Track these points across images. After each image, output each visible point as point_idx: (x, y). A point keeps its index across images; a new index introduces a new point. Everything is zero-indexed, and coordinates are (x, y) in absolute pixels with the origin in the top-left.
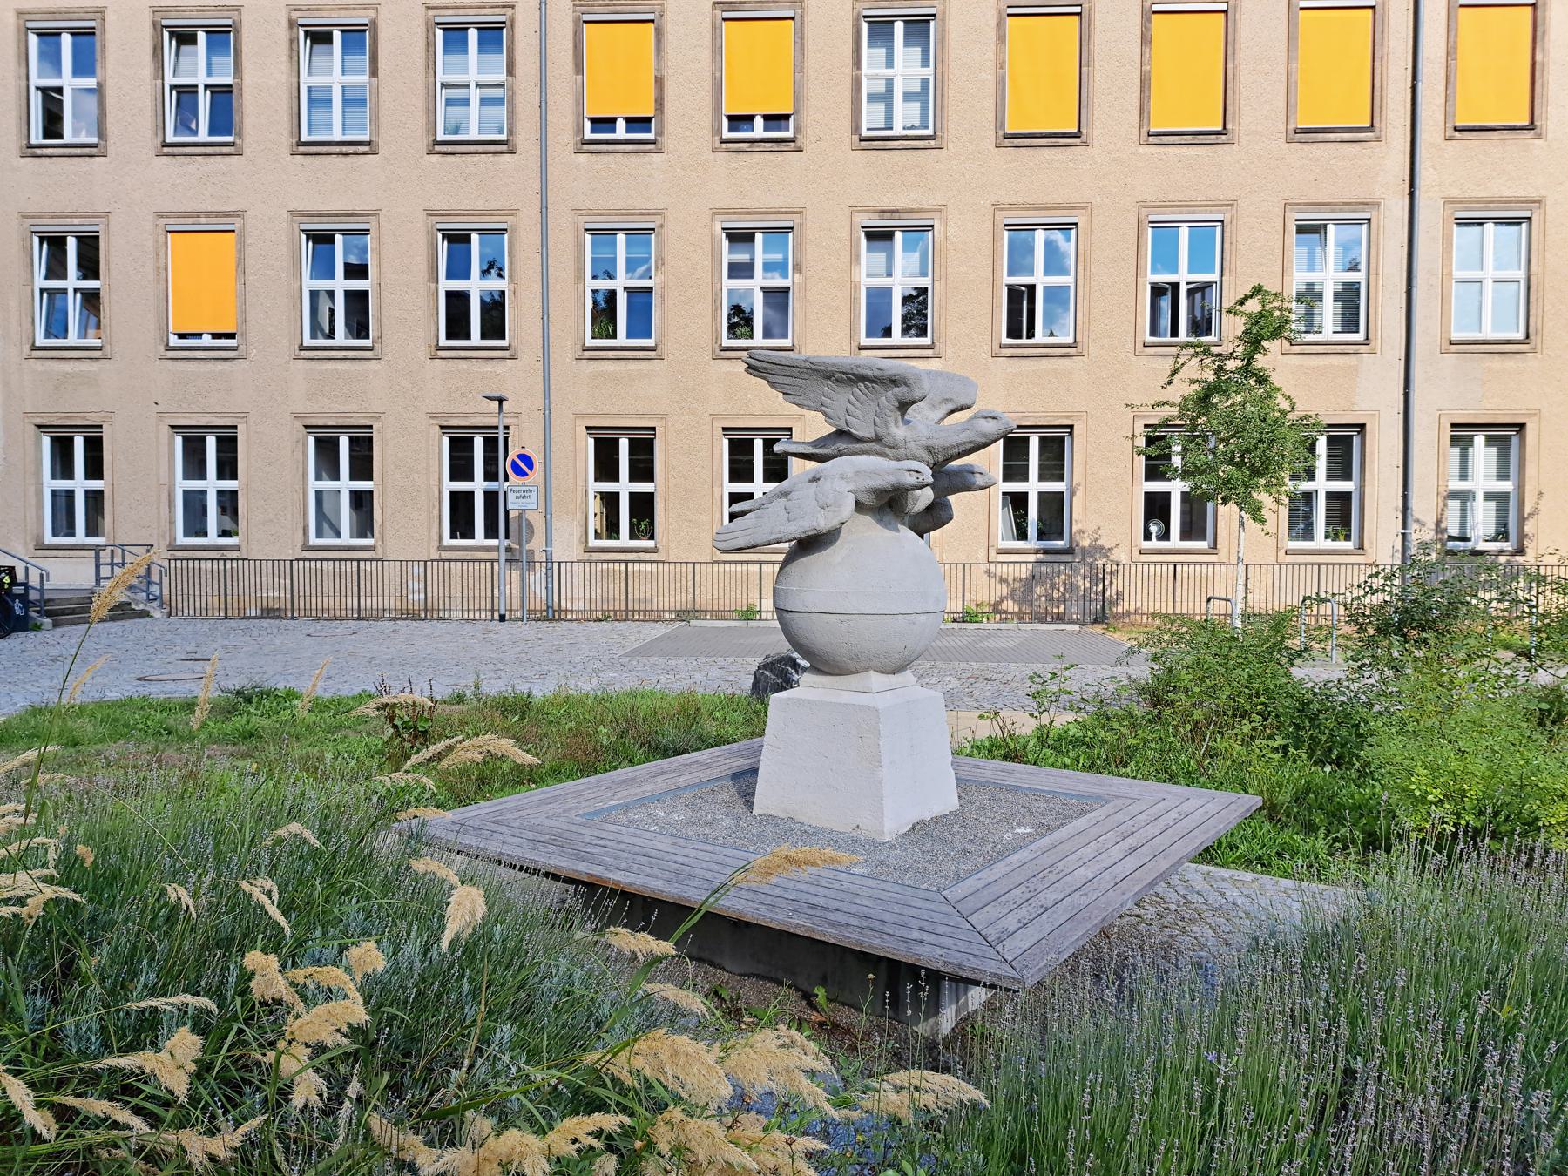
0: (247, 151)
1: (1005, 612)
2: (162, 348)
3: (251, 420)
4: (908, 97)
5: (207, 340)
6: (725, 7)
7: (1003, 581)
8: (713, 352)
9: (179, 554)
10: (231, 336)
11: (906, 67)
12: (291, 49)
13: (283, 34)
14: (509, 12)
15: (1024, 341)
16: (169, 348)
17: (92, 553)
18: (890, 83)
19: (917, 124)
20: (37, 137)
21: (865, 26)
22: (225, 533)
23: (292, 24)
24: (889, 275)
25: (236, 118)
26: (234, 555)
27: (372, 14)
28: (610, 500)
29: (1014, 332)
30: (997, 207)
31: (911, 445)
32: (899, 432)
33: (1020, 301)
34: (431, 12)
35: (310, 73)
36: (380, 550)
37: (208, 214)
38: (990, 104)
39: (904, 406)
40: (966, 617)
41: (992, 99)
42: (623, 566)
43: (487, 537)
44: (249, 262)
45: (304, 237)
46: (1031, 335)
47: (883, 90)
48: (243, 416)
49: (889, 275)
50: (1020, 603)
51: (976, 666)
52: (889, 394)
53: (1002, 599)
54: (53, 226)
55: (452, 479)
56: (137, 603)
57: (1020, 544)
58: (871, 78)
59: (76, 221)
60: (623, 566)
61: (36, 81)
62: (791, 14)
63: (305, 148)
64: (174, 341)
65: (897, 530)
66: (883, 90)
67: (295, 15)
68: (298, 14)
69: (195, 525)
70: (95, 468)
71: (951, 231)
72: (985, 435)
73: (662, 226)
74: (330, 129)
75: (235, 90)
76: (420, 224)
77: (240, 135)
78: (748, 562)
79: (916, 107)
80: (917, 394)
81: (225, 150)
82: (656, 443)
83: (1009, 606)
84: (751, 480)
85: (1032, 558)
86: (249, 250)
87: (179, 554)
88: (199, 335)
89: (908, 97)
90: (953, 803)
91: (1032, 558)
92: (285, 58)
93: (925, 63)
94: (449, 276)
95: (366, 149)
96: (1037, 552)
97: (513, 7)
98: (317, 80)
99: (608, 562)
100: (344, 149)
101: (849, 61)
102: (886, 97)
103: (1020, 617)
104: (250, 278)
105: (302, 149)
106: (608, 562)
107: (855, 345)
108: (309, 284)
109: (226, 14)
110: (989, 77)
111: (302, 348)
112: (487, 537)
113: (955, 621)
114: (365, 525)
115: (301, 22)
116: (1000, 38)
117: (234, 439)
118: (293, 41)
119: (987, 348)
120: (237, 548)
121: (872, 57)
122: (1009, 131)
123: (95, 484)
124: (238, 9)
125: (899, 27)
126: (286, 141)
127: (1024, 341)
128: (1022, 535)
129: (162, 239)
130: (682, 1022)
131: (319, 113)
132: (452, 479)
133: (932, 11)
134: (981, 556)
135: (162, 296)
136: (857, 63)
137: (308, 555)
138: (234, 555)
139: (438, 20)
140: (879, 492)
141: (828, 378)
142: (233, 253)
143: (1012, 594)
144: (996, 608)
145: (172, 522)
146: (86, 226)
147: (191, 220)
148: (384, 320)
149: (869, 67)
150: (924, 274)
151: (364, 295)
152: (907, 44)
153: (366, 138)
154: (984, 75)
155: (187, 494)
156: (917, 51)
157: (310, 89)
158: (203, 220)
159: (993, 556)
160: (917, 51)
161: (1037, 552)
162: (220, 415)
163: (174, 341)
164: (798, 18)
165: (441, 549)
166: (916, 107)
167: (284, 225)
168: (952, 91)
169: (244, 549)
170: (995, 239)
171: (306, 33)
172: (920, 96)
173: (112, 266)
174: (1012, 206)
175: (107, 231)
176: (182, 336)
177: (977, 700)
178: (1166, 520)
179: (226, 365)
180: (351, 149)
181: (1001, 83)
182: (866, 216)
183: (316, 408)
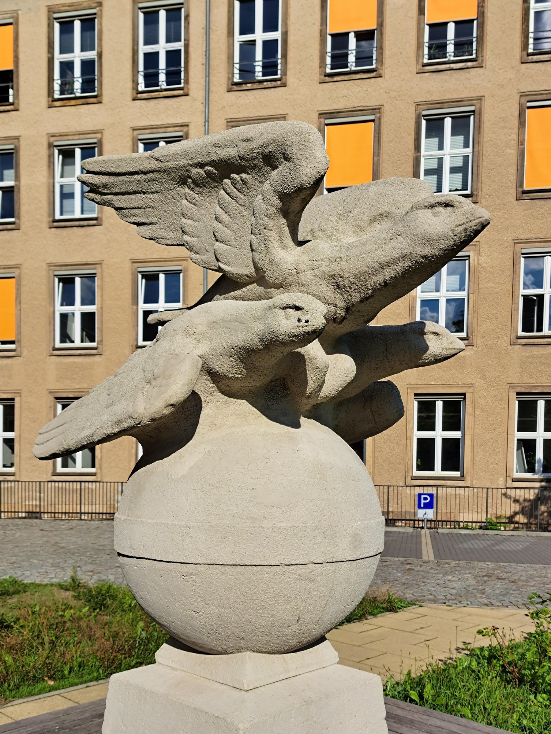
0: (23, 227)
1: (517, 523)
3: (23, 395)
4: (453, 170)
6: (327, 116)
7: (516, 501)
10: (12, 342)
11: (453, 149)
12: (49, 162)
13: (44, 152)
14: (185, 129)
15: (535, 334)
18: (440, 160)
19: (460, 188)
21: (424, 123)
23: (51, 146)
24: (437, 290)
25: (16, 207)
27: (99, 136)
29: (527, 327)
30: (517, 242)
31: (307, 277)
32: (286, 257)
33: (533, 306)
34: (136, 132)
35: (62, 176)
36: (99, 475)
38: (513, 170)
39: (294, 203)
40: (488, 526)
41: (515, 167)
44: (23, 296)
45: (56, 280)
46: (540, 329)
47: (435, 166)
48: (19, 393)
49: (437, 290)
50: (529, 518)
51: (491, 565)
52: (266, 186)
53: (516, 513)
57: (529, 475)
58: (427, 158)
62: (372, 117)
63: (57, 224)
65: (297, 425)
66: (435, 166)
67: (52, 139)
68: (53, 139)
71: (482, 259)
72: (428, 240)
74: (73, 212)
75: (15, 189)
76: (127, 267)
77: (19, 218)
78: (447, 487)
79: (459, 176)
80: (306, 174)
81: (9, 227)
83: (521, 518)
85: (537, 485)
86: (23, 289)
89: (453, 170)
91: (537, 485)
92: (45, 167)
93: (466, 145)
94: (146, 302)
95: (94, 222)
96: (541, 481)
97: (187, 126)
98: (65, 181)
100: (81, 223)
101: (412, 146)
102: (437, 172)
103: (528, 526)
104: (23, 306)
105: (56, 224)
108: (60, 309)
109: (11, 141)
110: (512, 152)
113: (481, 528)
115: (56, 143)
116: (522, 123)
118: (51, 157)
119: (507, 339)
120: (13, 474)
121: (428, 146)
122: (526, 188)
124: (17, 138)
125: (448, 122)
126: (45, 219)
127: (535, 334)
128: (531, 469)
131: (66, 202)
133: (472, 108)
134: (501, 482)
136: (417, 147)
139: (141, 137)
140: (247, 355)
141: (183, 182)
142: (14, 291)
143: (523, 511)
144: (511, 519)
148: (104, 330)
149: (426, 151)
150: (461, 289)
151: (93, 314)
152: (453, 134)
153: (94, 215)
154: (509, 151)
156: (460, 139)
157: (62, 186)
159: (510, 483)
160: (461, 138)
161: (541, 481)
164: (377, 121)
166: (459, 176)
167: (44, 273)
168: (485, 163)
170: (515, 264)
171: (59, 150)
172: (460, 170)
174: (528, 241)
177: (488, 597)
180: (85, 223)
181: (521, 155)
183: (62, 386)
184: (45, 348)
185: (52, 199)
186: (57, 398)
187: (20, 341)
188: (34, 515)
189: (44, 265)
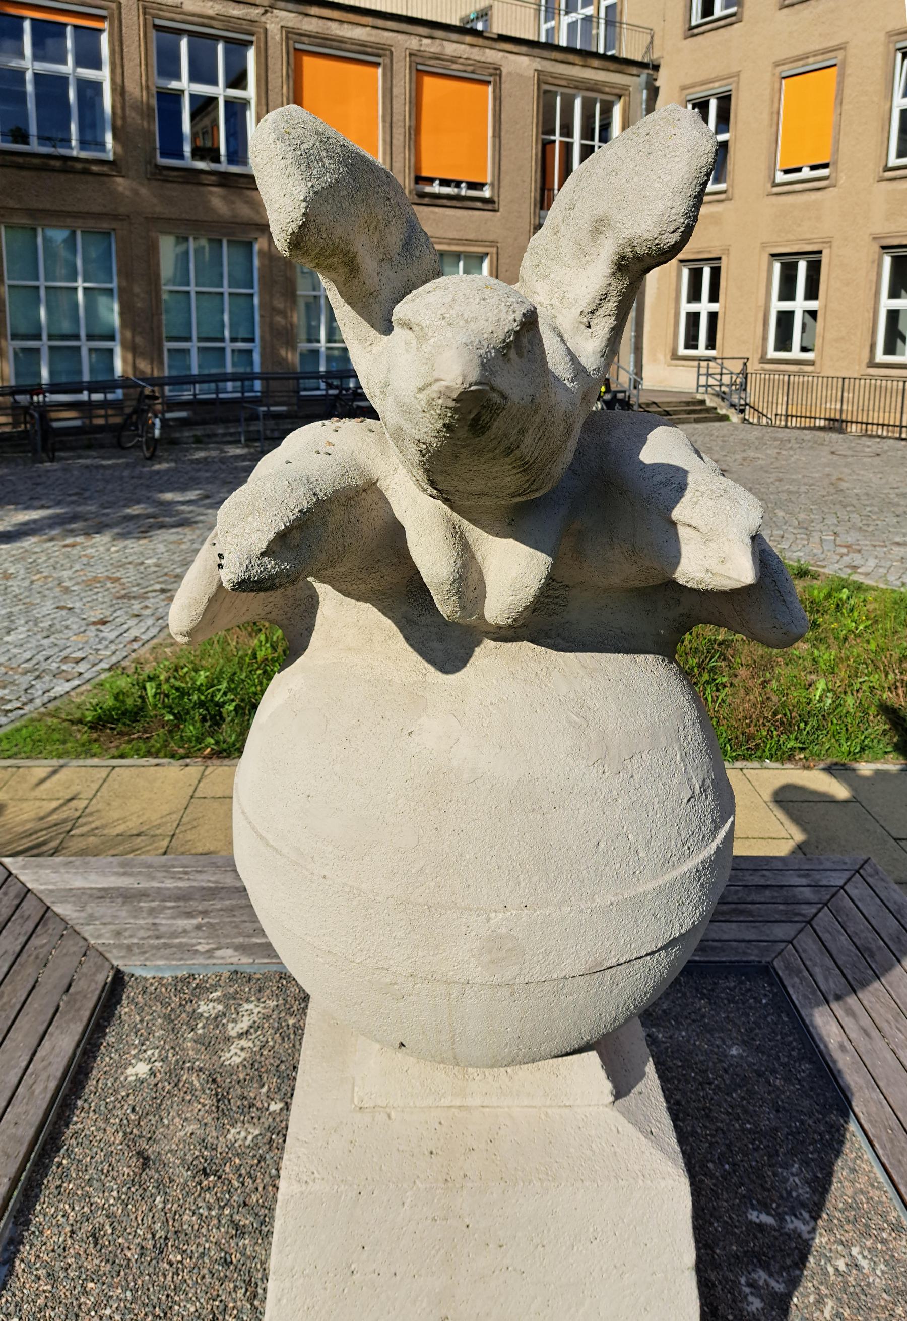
2: (769, 185)
5: (806, 173)
10: (825, 166)
16: (775, 185)
17: (696, 363)
20: (696, 19)
22: (804, 349)
28: (694, 318)
43: (707, 348)
44: (847, 92)
54: (699, 93)
56: (721, 409)
59: (716, 84)
61: (104, 75)
64: (780, 177)
70: (812, 293)
88: (799, 170)
90: (592, 1057)
111: (887, 169)
112: (707, 348)
120: (812, 363)
123: (714, 307)
129: (777, 86)
130: (139, 670)
135: (774, 138)
142: (834, 85)
145: (765, 339)
146: (719, 87)
147: (801, 63)
155: (689, 314)
163: (780, 177)
165: (764, 360)
169: (818, 364)
173: (739, 118)
175: (738, 89)
176: (786, 172)
179: (819, 194)
184: (873, 168)
185: (688, 17)
186: (884, 247)
187: (836, 163)
188: (836, 425)
189: (882, 37)
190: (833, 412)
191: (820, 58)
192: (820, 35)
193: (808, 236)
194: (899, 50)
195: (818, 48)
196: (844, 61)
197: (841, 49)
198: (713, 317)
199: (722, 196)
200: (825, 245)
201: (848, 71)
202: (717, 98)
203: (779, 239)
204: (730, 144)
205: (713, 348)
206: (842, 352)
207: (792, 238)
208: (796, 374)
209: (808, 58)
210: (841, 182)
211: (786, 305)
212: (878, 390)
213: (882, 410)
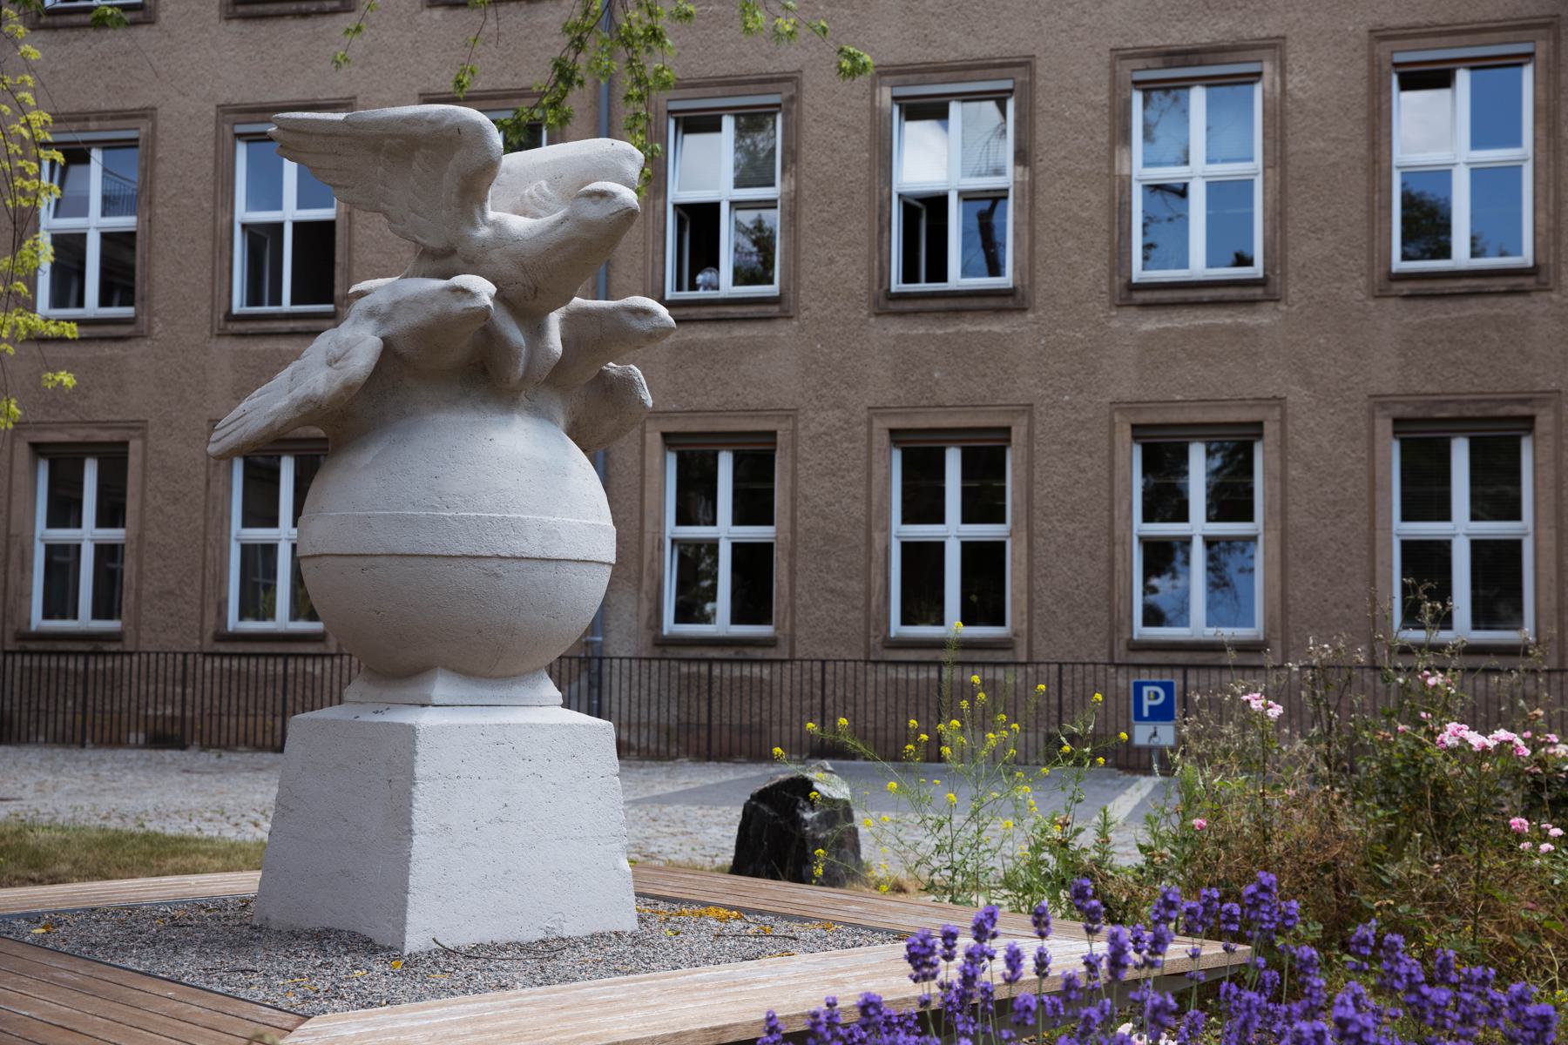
8: (877, 302)
9: (32, 646)
15: (266, 309)
26: (114, 647)
37: (101, 115)
42: (934, 674)
48: (140, 427)
55: (1405, 517)
60: (704, 668)
69: (922, 596)
70: (111, 514)
73: (792, 99)
82: (777, 455)
84: (966, 519)
87: (32, 646)
99: (231, 655)
106: (240, 655)
107: (1379, 272)
111: (230, 317)
114: (984, 601)
117: (124, 459)
132: (1405, 517)
137: (222, 648)
138: (114, 647)
158: (93, 125)
162: (105, 425)
178: (1443, 591)
179: (116, 350)
182: (1139, 63)
190: (168, 725)
191: (109, 124)
192: (107, 87)
193: (102, 416)
194: (1396, 65)
195: (103, 106)
196: (152, 136)
197: (144, 116)
198: (107, 555)
199: (774, 310)
200: (132, 433)
201: (1041, 100)
202: (737, 116)
203: (46, 419)
204: (139, 237)
205: (764, 617)
206: (171, 615)
207: (73, 417)
208: (96, 653)
209: (87, 119)
210: (156, 330)
211: (923, 532)
212: (235, 677)
213: (242, 713)
